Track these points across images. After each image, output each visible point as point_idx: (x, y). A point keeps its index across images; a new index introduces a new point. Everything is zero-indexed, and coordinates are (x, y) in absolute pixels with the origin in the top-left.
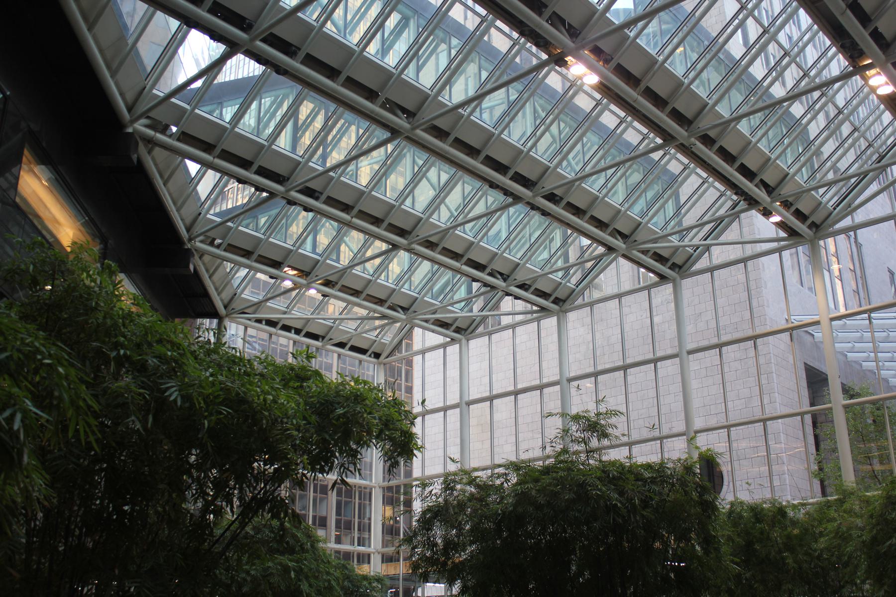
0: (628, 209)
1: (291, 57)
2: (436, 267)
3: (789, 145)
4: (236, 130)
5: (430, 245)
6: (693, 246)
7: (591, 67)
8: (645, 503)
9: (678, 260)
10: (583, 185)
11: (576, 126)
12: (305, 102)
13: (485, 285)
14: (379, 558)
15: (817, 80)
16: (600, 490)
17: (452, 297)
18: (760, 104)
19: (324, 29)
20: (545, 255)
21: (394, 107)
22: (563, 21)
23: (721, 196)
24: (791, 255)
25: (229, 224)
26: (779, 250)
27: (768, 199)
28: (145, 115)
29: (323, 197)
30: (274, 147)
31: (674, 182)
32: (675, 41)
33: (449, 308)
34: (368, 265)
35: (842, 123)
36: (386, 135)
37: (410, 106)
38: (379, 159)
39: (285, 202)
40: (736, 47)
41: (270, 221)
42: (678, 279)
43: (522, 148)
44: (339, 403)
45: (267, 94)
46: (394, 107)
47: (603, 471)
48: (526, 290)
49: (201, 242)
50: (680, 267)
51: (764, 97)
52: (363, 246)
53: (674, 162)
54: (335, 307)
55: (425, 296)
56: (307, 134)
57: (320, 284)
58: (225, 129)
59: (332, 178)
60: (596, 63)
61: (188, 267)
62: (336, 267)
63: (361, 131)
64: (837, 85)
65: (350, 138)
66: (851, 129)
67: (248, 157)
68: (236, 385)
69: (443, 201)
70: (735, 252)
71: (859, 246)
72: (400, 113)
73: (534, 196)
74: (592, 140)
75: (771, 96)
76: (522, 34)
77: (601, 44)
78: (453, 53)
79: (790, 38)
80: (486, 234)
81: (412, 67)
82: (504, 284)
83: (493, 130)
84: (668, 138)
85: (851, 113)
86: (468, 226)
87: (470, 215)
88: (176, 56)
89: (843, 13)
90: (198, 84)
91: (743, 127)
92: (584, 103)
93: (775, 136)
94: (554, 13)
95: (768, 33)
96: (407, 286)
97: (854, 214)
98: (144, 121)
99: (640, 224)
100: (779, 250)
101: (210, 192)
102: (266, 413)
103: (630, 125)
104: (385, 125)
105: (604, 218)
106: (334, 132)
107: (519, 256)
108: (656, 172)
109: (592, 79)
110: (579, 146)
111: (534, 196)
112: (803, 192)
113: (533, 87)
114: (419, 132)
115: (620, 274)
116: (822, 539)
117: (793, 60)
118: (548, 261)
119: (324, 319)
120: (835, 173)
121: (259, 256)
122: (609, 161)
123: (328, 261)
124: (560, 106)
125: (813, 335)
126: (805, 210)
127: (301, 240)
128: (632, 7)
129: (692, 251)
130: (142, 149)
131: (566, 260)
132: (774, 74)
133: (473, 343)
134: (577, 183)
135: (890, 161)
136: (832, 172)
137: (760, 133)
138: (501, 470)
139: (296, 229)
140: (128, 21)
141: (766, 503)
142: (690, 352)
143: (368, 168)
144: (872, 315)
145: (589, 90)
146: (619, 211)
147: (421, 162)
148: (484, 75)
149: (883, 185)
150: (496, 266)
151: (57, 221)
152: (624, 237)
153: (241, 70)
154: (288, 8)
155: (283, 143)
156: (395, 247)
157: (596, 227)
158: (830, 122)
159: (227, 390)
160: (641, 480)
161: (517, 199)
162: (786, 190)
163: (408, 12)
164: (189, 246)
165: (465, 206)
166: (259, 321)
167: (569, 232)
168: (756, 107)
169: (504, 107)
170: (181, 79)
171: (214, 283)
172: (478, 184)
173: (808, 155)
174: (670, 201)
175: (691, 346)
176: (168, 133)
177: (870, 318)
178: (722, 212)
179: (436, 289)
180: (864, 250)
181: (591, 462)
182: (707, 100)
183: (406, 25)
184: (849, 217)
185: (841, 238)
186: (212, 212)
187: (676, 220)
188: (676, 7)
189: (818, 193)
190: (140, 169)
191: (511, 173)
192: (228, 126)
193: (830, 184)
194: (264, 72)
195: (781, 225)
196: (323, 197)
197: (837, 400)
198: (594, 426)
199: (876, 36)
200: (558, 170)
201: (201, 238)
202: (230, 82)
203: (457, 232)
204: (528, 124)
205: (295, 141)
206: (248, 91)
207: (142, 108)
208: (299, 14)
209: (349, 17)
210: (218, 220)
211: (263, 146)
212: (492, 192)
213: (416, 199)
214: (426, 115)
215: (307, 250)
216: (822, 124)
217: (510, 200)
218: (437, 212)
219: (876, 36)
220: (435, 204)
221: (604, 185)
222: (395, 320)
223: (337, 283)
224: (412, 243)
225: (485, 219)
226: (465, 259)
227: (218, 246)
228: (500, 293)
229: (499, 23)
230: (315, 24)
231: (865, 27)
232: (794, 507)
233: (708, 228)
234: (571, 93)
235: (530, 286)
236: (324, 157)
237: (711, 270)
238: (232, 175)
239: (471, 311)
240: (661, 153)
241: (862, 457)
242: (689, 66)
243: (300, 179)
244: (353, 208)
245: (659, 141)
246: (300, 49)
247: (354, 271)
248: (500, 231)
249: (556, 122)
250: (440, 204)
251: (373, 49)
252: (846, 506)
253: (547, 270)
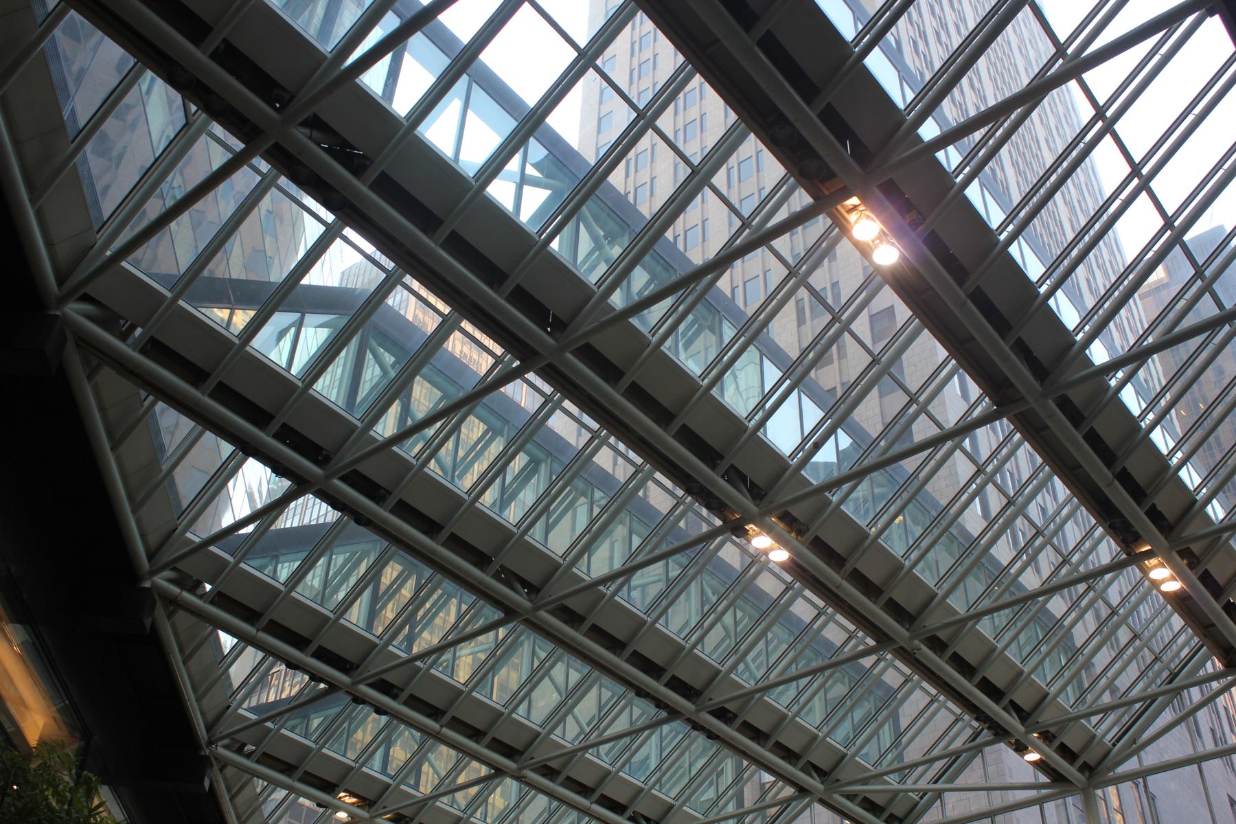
0: (827, 735)
1: (378, 503)
2: (555, 804)
3: (1047, 654)
4: (293, 594)
6: (918, 791)
7: (782, 541)
10: (766, 698)
11: (757, 616)
15: (1082, 569)
18: (1007, 598)
19: (426, 470)
20: (710, 794)
21: (511, 578)
22: (743, 478)
23: (957, 721)
24: (1057, 806)
25: (269, 724)
26: (1040, 801)
27: (1021, 728)
28: (171, 565)
29: (404, 695)
30: (342, 621)
31: (890, 699)
32: (893, 509)
34: (459, 796)
35: (1117, 626)
36: (498, 615)
37: (532, 578)
38: (485, 647)
39: (349, 698)
40: (973, 520)
41: (326, 723)
43: (683, 643)
45: (341, 549)
46: (511, 578)
49: (226, 747)
51: (1012, 589)
52: (454, 768)
53: (891, 671)
56: (390, 606)
58: (278, 592)
59: (419, 669)
60: (786, 534)
61: (202, 782)
62: (414, 796)
63: (464, 607)
64: (1107, 577)
65: (448, 614)
66: (1129, 635)
67: (305, 633)
69: (570, 711)
71: (1152, 799)
72: (519, 586)
73: (698, 711)
74: (779, 637)
75: (1021, 587)
76: (688, 491)
77: (795, 511)
78: (596, 511)
79: (1044, 510)
80: (628, 760)
81: (540, 526)
83: (645, 617)
84: (884, 640)
85: (1129, 613)
86: (604, 749)
87: (607, 733)
88: (224, 491)
89: (1110, 485)
90: (250, 529)
91: (985, 627)
92: (769, 585)
93: (1028, 641)
94: (732, 466)
95: (1015, 505)
97: (1142, 753)
98: (168, 573)
100: (1040, 801)
101: (251, 677)
103: (831, 619)
104: (496, 602)
105: (795, 746)
106: (428, 605)
107: (673, 794)
108: (867, 684)
109: (780, 555)
110: (761, 644)
111: (698, 711)
112: (1069, 720)
113: (701, 561)
114: (543, 614)
117: (1049, 541)
118: (715, 803)
120: (1112, 693)
121: (306, 772)
122: (802, 666)
123: (403, 787)
124: (738, 589)
126: (1074, 746)
127: (367, 754)
128: (835, 460)
129: (917, 798)
130: (160, 612)
131: (740, 803)
132: (1024, 557)
134: (758, 695)
135: (1185, 682)
136: (1108, 692)
137: (1008, 636)
139: (363, 736)
140: (166, 439)
143: (469, 659)
145: (777, 570)
146: (815, 737)
147: (543, 655)
148: (636, 541)
149: (1180, 715)
151: (23, 704)
152: (822, 774)
153: (308, 512)
154: (381, 439)
155: (356, 616)
156: (499, 772)
158: (1102, 625)
161: (674, 713)
162: (1046, 717)
163: (541, 455)
164: (207, 752)
165: (601, 720)
167: (745, 763)
168: (1001, 602)
169: (661, 586)
170: (227, 521)
171: (235, 808)
172: (620, 689)
173: (1073, 669)
174: (886, 726)
176: (199, 592)
178: (957, 744)
180: (1159, 802)
182: (935, 589)
183: (535, 470)
184: (1135, 758)
185: (1127, 786)
186: (245, 705)
187: (895, 752)
188: (893, 466)
189: (1089, 722)
190: (154, 640)
191: (666, 677)
192: (282, 588)
193: (1106, 710)
194: (339, 521)
195: (1040, 765)
196: (404, 695)
199: (1154, 515)
200: (732, 676)
201: (226, 741)
202: (292, 529)
203: (587, 755)
204: (693, 613)
205: (372, 614)
206: (314, 543)
207: (168, 555)
208: (395, 448)
209: (461, 453)
210: (254, 717)
211: (327, 619)
212: (639, 701)
213: (534, 703)
214: (555, 592)
215: (374, 768)
216: (1092, 627)
217: (664, 714)
218: (561, 726)
219: (1154, 515)
220: (559, 715)
221: (796, 699)
224: (524, 768)
225: (628, 739)
226: (596, 795)
227: (249, 756)
229: (658, 476)
230: (414, 461)
231: (1139, 504)
233: (939, 765)
234: (752, 571)
236: (410, 639)
238: (280, 657)
240: (873, 658)
242: (911, 543)
243: (374, 668)
244: (444, 713)
245: (871, 642)
246: (390, 493)
247: (438, 804)
248: (648, 757)
249: (731, 610)
250: (565, 715)
251: (489, 498)
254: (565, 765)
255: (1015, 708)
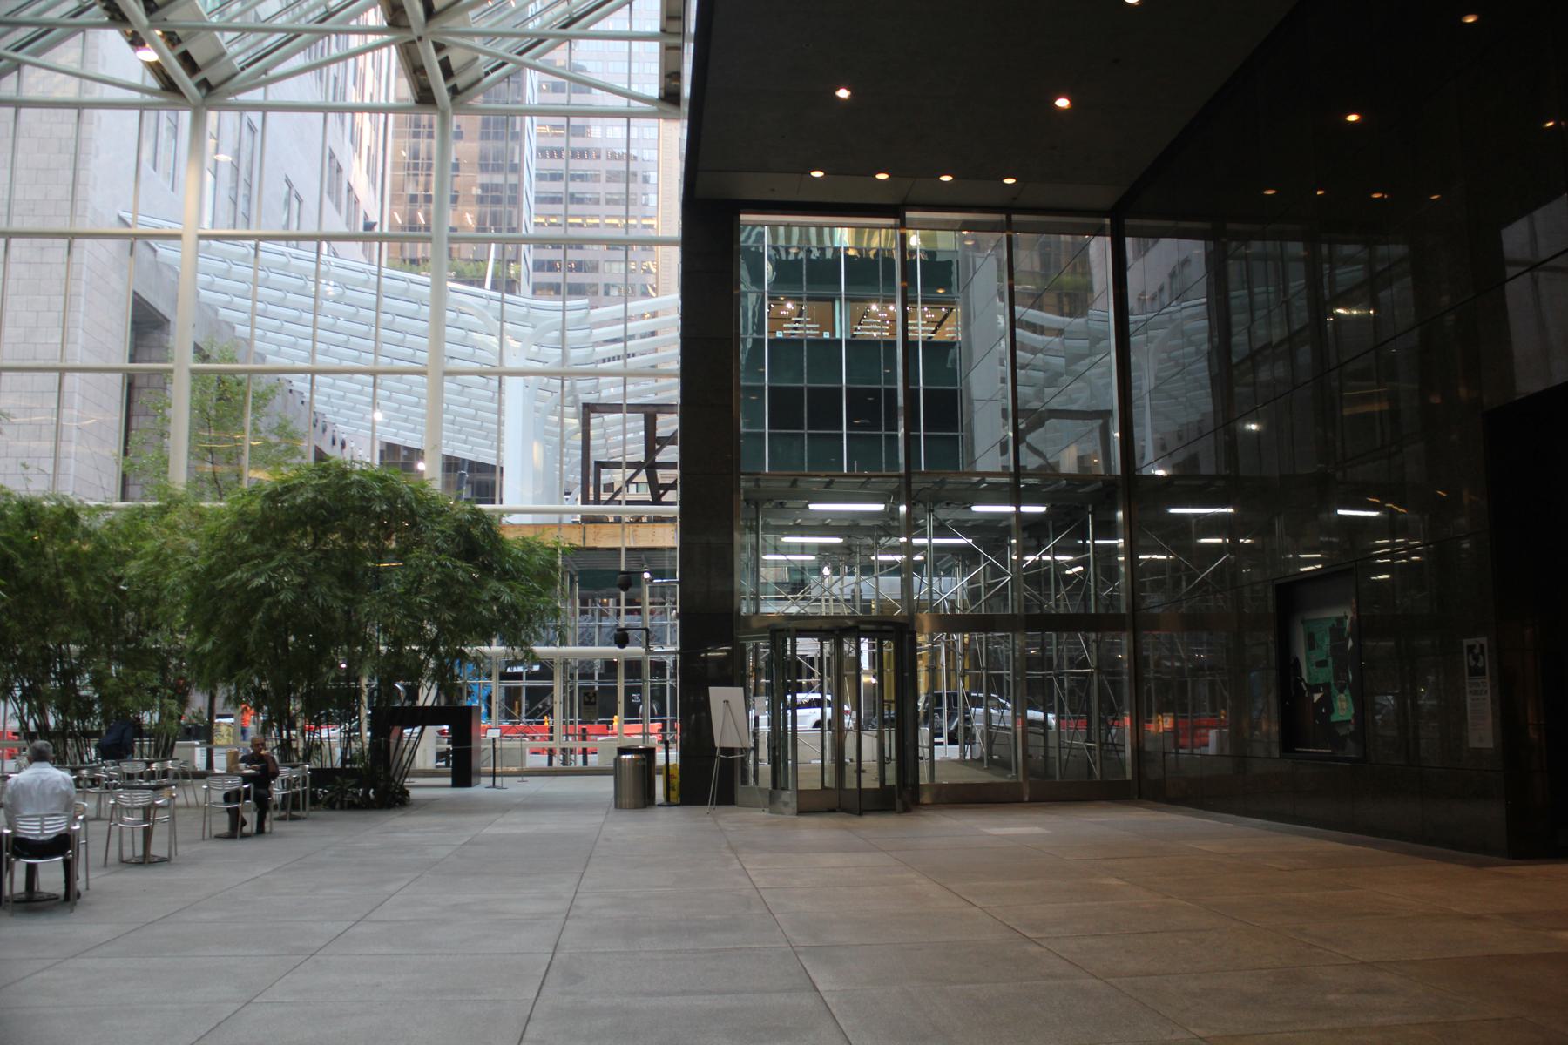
12: (1201, 243)
27: (145, 21)
70: (68, 89)
112: (204, 28)
125: (155, 251)
141: (48, 499)
149: (314, 61)
177: (257, 248)
195: (156, 69)
232: (91, 511)
233: (22, 33)
252: (169, 518)
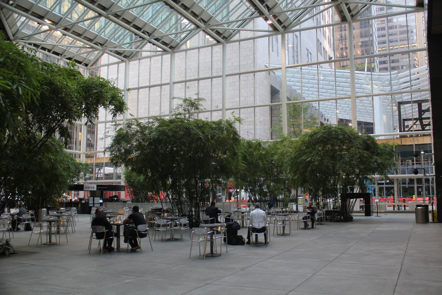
5: (117, 16)
6: (233, 30)
8: (212, 138)
9: (226, 35)
13: (141, 37)
14: (84, 155)
16: (195, 131)
17: (123, 42)
26: (269, 36)
27: (268, 13)
33: (122, 46)
42: (225, 43)
44: (94, 87)
47: (197, 124)
48: (158, 41)
50: (226, 38)
54: (68, 40)
55: (111, 39)
57: (63, 29)
62: (71, 22)
68: (49, 76)
70: (250, 35)
82: (149, 38)
96: (103, 34)
99: (212, 17)
102: (64, 90)
112: (283, 12)
115: (201, 38)
116: (276, 156)
119: (62, 46)
121: (33, 12)
123: (67, 19)
131: (177, 30)
133: (131, 63)
138: (151, 120)
142: (227, 76)
144: (303, 67)
146: (204, 10)
150: (146, 29)
152: (204, 22)
156: (100, 15)
157: (193, 16)
159: (45, 78)
160: (211, 128)
162: (276, 10)
166: (30, 44)
171: (8, 23)
174: (225, 10)
175: (227, 73)
177: (301, 69)
179: (116, 37)
181: (191, 119)
187: (227, 18)
195: (272, 25)
197: (284, 102)
198: (193, 105)
215: (56, 12)
222: (97, 50)
223: (70, 30)
224: (109, 14)
226: (132, 24)
227: (11, 5)
228: (146, 41)
232: (264, 143)
233: (240, 23)
235: (160, 40)
237: (239, 41)
239: (131, 48)
241: (290, 125)
247: (79, 25)
253: (168, 33)
254: (123, 13)
255: (267, 7)
